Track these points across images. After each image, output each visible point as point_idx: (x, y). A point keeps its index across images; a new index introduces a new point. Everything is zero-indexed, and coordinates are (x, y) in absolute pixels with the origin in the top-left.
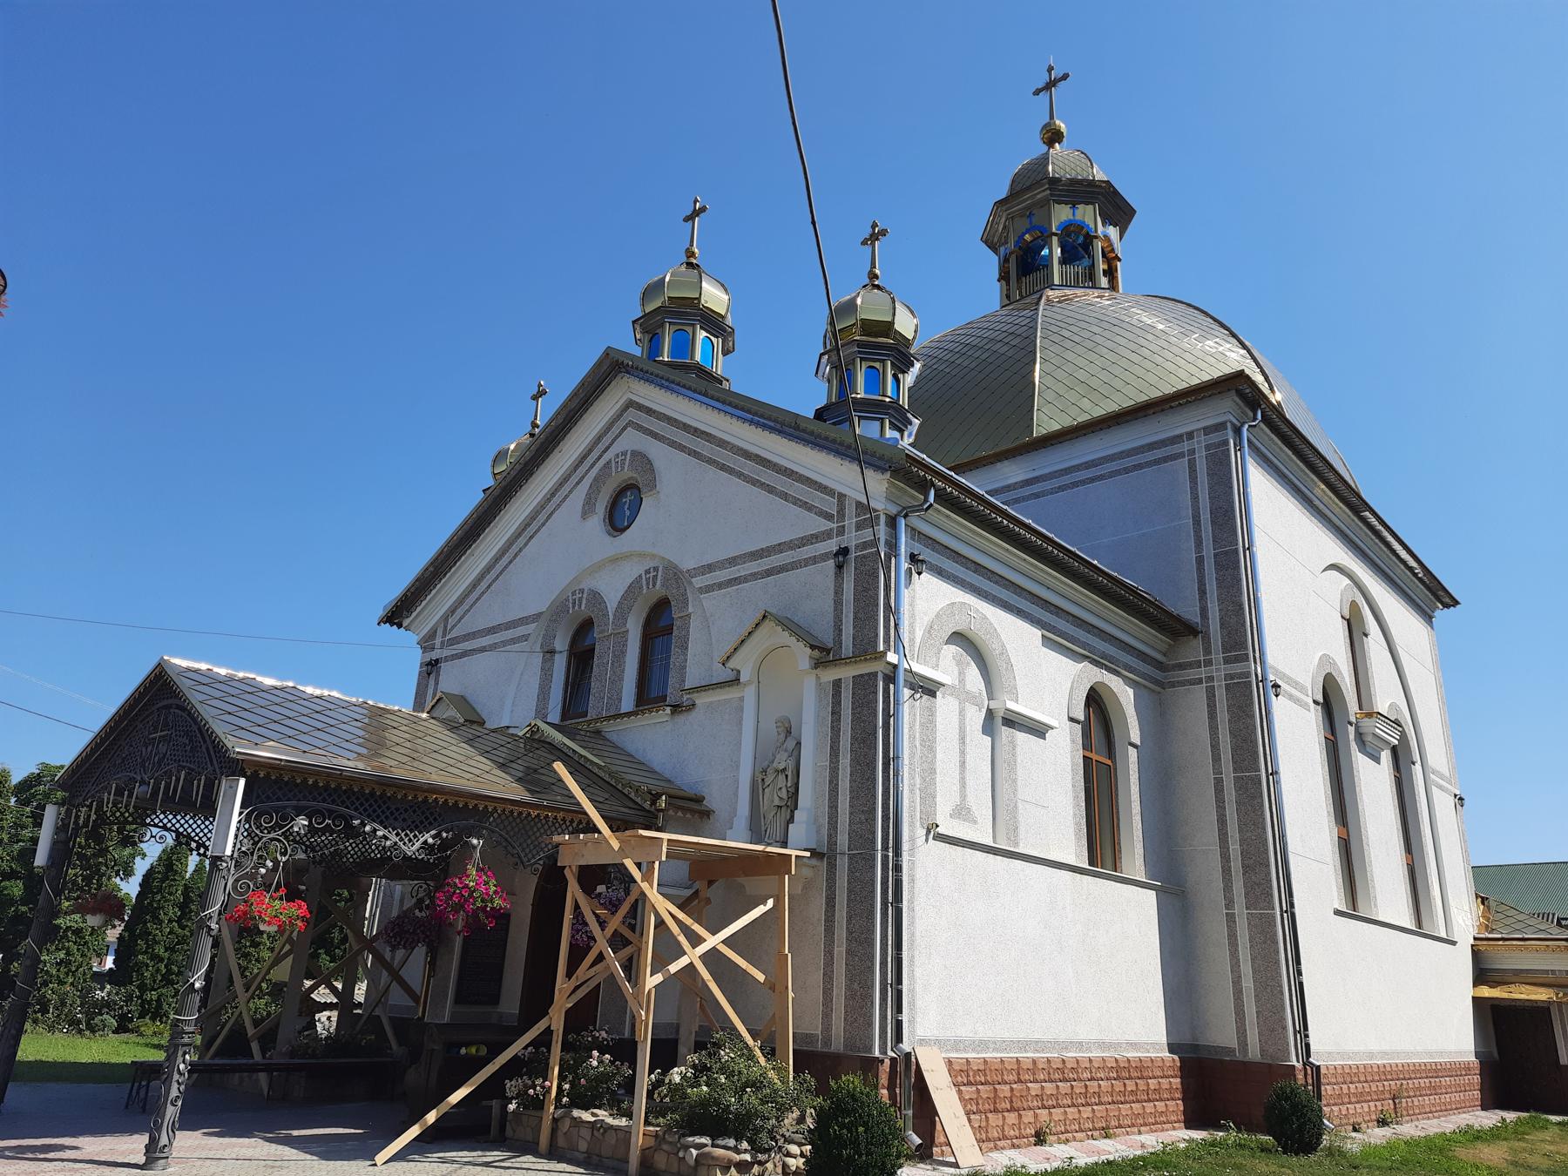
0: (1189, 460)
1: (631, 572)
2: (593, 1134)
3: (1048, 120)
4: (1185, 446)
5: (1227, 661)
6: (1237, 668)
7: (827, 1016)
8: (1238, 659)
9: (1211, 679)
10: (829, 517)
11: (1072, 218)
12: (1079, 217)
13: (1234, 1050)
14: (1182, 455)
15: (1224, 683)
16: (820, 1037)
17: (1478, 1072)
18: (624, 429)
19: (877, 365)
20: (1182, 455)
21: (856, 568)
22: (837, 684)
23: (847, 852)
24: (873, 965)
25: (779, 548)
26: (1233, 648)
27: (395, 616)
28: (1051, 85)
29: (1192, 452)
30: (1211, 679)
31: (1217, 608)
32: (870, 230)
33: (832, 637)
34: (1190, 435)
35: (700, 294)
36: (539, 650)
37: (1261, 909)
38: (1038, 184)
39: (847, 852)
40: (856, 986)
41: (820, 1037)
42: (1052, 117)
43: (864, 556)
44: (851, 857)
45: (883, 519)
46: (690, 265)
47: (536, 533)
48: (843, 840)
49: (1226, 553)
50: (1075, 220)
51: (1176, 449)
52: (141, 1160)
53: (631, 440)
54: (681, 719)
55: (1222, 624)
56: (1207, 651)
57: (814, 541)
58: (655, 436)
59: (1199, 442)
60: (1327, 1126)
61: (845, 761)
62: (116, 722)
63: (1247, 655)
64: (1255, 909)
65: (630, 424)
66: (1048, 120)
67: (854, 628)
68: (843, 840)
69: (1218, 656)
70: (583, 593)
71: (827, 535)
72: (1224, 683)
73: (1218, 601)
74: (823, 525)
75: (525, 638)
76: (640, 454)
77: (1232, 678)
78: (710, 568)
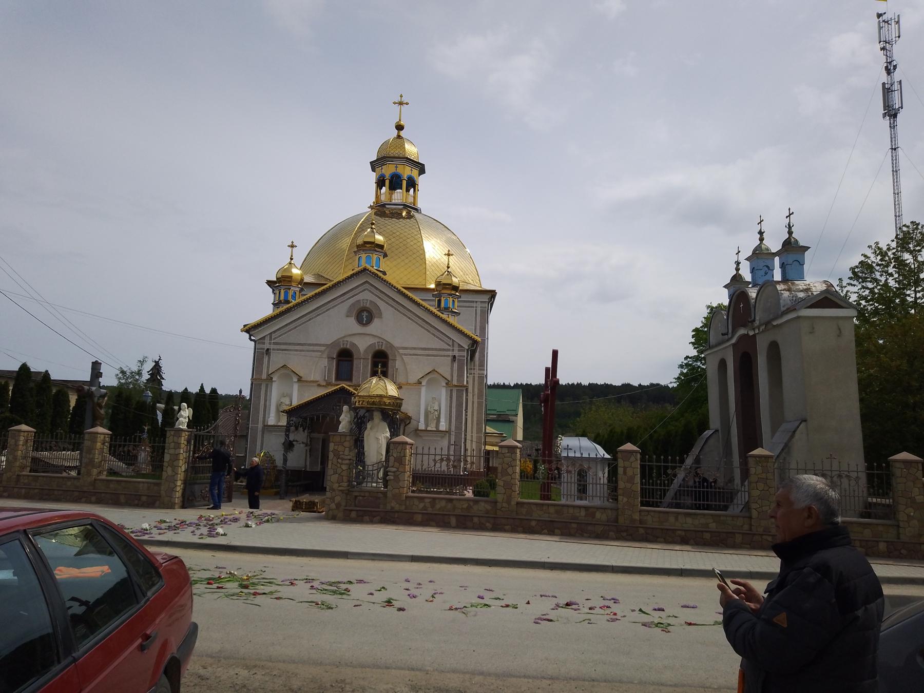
1: (370, 341)
4: (475, 305)
5: (479, 369)
6: (481, 372)
9: (474, 374)
10: (449, 345)
14: (473, 307)
17: (494, 466)
18: (365, 290)
19: (454, 299)
29: (476, 307)
34: (476, 302)
48: (453, 428)
51: (471, 304)
56: (474, 366)
60: (108, 467)
61: (454, 410)
62: (314, 401)
65: (367, 289)
68: (453, 428)
69: (477, 368)
71: (449, 350)
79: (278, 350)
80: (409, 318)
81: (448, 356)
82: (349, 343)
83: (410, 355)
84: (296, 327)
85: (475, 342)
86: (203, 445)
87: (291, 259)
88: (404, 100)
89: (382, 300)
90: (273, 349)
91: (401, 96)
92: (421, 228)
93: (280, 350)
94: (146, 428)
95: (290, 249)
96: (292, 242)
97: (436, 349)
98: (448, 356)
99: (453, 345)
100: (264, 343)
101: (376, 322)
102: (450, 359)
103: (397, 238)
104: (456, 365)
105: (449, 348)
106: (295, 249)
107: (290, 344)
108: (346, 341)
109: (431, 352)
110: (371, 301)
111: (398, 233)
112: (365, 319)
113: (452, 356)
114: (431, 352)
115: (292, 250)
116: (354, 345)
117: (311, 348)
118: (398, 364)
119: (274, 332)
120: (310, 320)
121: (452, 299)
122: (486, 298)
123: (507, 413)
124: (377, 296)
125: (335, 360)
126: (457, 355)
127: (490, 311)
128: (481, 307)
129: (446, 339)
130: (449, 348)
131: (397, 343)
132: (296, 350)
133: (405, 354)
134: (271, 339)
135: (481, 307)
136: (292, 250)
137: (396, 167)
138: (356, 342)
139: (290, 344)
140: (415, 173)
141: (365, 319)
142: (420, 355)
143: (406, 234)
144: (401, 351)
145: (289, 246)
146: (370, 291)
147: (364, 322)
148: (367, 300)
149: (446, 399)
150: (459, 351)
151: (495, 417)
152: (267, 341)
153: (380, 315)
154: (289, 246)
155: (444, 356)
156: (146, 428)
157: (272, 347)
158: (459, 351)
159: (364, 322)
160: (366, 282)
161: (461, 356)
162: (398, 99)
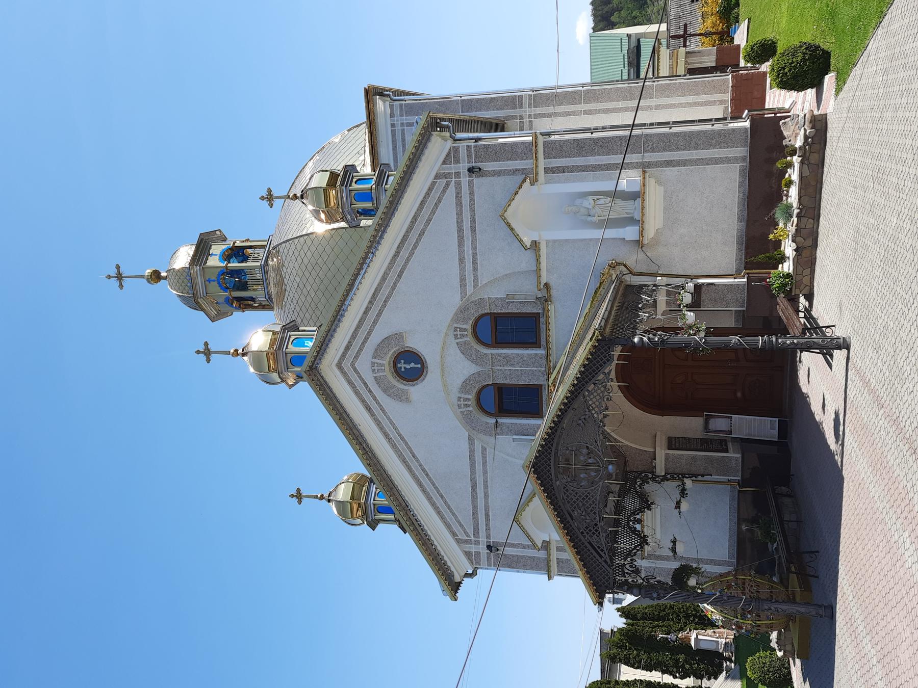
0: (406, 126)
1: (455, 355)
2: (804, 216)
3: (144, 280)
4: (398, 128)
5: (521, 107)
6: (526, 101)
7: (728, 160)
8: (521, 101)
10: (448, 184)
11: (218, 256)
12: (218, 252)
13: (733, 43)
14: (403, 131)
15: (533, 109)
16: (741, 164)
18: (355, 370)
19: (354, 180)
20: (403, 131)
21: (482, 162)
22: (547, 170)
23: (642, 154)
24: (702, 131)
25: (460, 223)
26: (515, 104)
27: (453, 587)
28: (120, 277)
29: (402, 124)
30: (530, 116)
31: (492, 112)
32: (202, 355)
33: (520, 176)
35: (321, 188)
36: (492, 439)
37: (653, 91)
38: (191, 280)
39: (642, 154)
40: (714, 141)
41: (741, 164)
42: (142, 277)
43: (476, 156)
44: (645, 151)
45: (454, 145)
46: (302, 197)
47: (411, 452)
49: (462, 106)
50: (220, 255)
52: (845, 351)
53: (364, 364)
54: (553, 299)
55: (501, 109)
56: (514, 117)
57: (460, 196)
58: (366, 339)
59: (397, 120)
61: (592, 160)
63: (519, 96)
64: (653, 94)
66: (144, 280)
67: (516, 160)
69: (517, 112)
70: (460, 398)
71: (458, 185)
72: (533, 109)
73: (488, 111)
74: (452, 189)
75: (484, 450)
76: (376, 350)
77: (531, 104)
78: (463, 280)
79: (488, 529)
80: (400, 276)
81: (471, 184)
82: (463, 396)
83: (475, 269)
84: (442, 496)
85: (434, 125)
86: (681, 655)
87: (322, 497)
88: (113, 272)
89: (369, 334)
90: (488, 537)
91: (109, 277)
92: (285, 239)
93: (487, 525)
94: (660, 636)
95: (304, 500)
96: (292, 496)
97: (459, 214)
98: (471, 184)
99: (446, 176)
100: (478, 554)
101: (413, 343)
102: (477, 181)
103: (304, 280)
104: (488, 166)
105: (453, 184)
106: (304, 492)
107: (475, 507)
108: (459, 401)
109: (467, 226)
110: (374, 357)
111: (298, 279)
112: (412, 365)
113: (469, 177)
114: (467, 226)
115: (305, 497)
116: (465, 386)
117: (479, 467)
118: (497, 293)
119: (454, 534)
120: (424, 470)
121: (353, 184)
122: (380, 105)
123: (625, 52)
124: (364, 343)
125: (500, 420)
126: (467, 165)
127: (423, 94)
128: (401, 115)
129: (435, 195)
130: (453, 184)
131: (455, 301)
132: (486, 495)
133: (476, 280)
134: (468, 542)
135: (401, 115)
136: (305, 497)
137: (209, 281)
138: (459, 382)
139: (475, 507)
140: (217, 249)
141: (412, 365)
142: (474, 249)
143: (297, 266)
144: (470, 289)
145: (300, 502)
146: (356, 357)
147: (419, 366)
148: (373, 364)
149: (567, 181)
150: (457, 161)
151: (632, 70)
152: (473, 548)
153: (399, 336)
154: (300, 502)
155: (472, 194)
156: (660, 636)
157: (483, 539)
158: (457, 161)
159: (419, 366)
160: (339, 366)
161: (469, 156)
162: (114, 282)
